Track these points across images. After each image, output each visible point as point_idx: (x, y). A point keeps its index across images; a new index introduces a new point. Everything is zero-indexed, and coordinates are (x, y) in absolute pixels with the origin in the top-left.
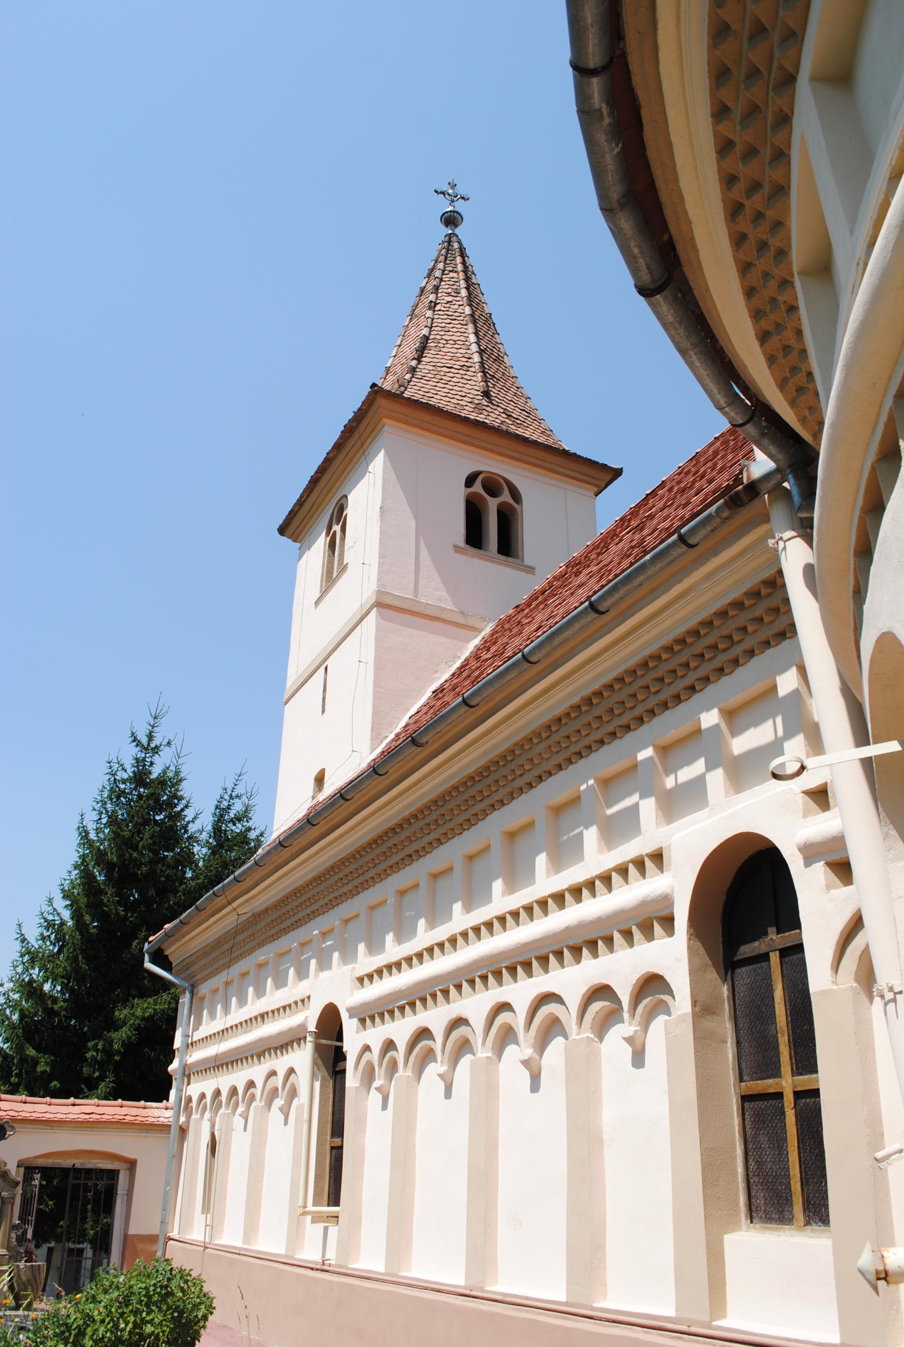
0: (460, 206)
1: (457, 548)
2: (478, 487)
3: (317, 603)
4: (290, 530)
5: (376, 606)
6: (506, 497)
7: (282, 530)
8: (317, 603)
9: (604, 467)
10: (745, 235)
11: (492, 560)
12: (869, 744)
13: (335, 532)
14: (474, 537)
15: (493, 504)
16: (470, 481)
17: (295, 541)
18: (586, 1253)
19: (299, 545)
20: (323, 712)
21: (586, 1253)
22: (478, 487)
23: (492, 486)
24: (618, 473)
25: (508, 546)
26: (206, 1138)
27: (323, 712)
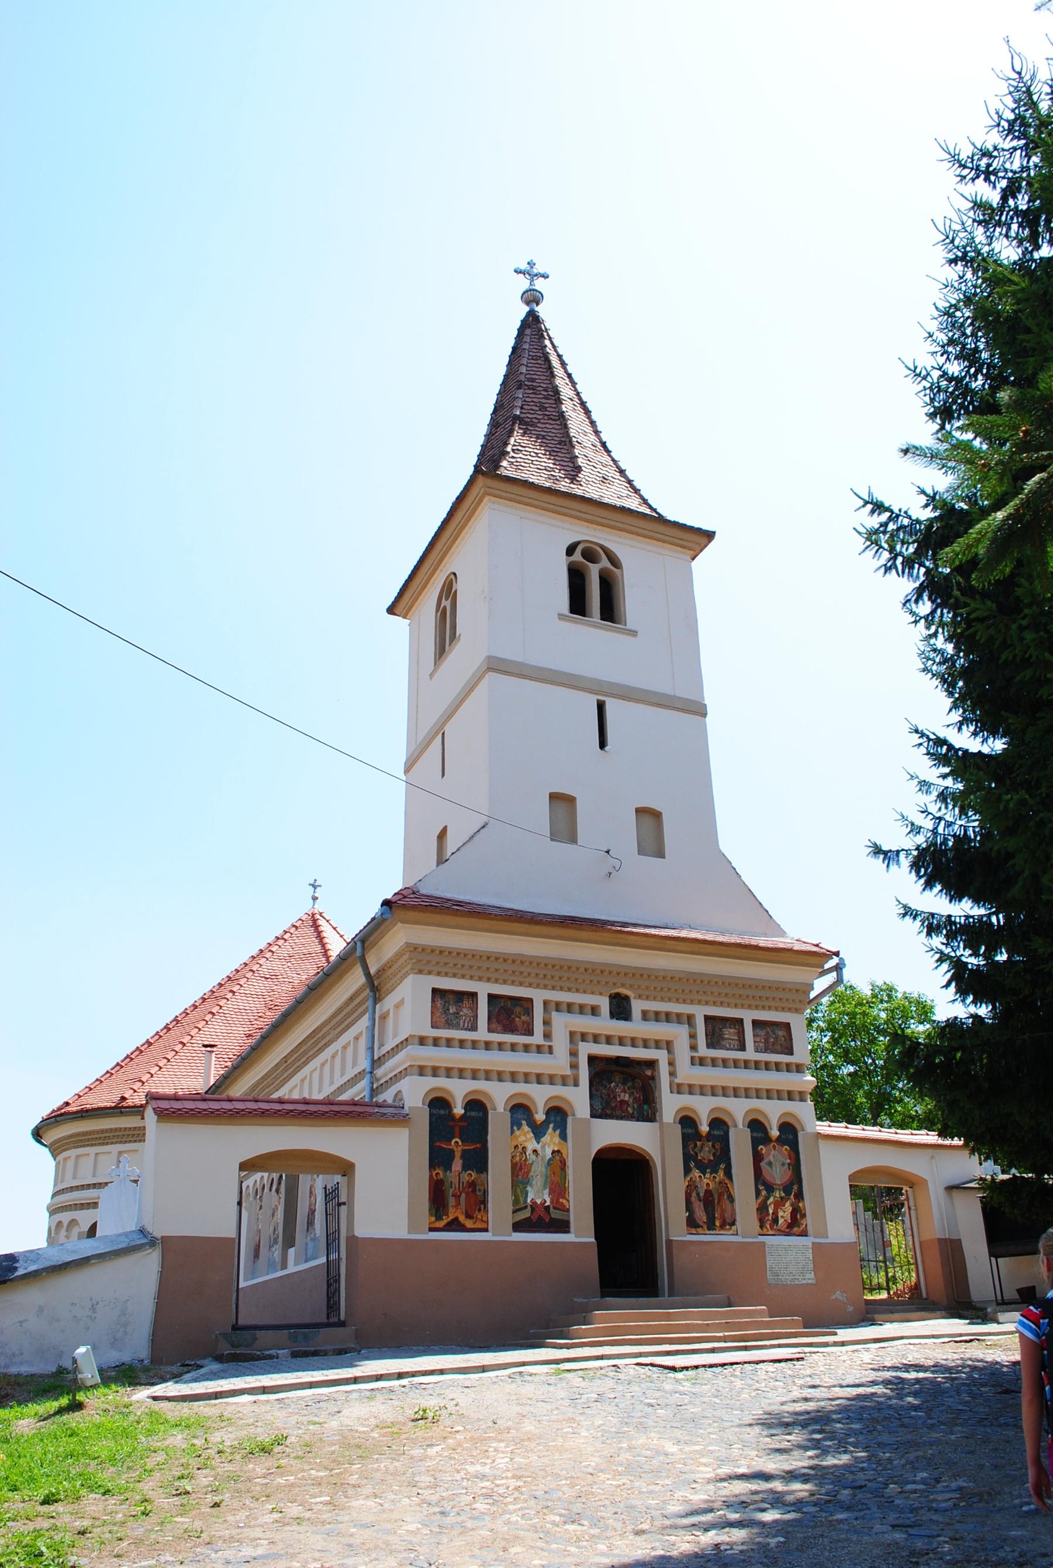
0: (540, 284)
1: (561, 616)
2: (577, 557)
3: (431, 675)
4: (399, 609)
5: (490, 669)
6: (605, 563)
7: (391, 610)
8: (431, 675)
9: (699, 531)
10: (550, 797)
11: (595, 626)
12: (162, 1237)
13: (445, 607)
14: (578, 605)
15: (594, 572)
16: (570, 550)
17: (405, 617)
18: (310, 1093)
19: (408, 621)
20: (443, 775)
21: (310, 1093)
22: (577, 557)
23: (590, 555)
24: (710, 535)
25: (610, 612)
26: (810, 1390)
27: (443, 775)
